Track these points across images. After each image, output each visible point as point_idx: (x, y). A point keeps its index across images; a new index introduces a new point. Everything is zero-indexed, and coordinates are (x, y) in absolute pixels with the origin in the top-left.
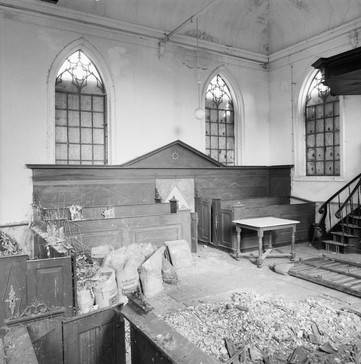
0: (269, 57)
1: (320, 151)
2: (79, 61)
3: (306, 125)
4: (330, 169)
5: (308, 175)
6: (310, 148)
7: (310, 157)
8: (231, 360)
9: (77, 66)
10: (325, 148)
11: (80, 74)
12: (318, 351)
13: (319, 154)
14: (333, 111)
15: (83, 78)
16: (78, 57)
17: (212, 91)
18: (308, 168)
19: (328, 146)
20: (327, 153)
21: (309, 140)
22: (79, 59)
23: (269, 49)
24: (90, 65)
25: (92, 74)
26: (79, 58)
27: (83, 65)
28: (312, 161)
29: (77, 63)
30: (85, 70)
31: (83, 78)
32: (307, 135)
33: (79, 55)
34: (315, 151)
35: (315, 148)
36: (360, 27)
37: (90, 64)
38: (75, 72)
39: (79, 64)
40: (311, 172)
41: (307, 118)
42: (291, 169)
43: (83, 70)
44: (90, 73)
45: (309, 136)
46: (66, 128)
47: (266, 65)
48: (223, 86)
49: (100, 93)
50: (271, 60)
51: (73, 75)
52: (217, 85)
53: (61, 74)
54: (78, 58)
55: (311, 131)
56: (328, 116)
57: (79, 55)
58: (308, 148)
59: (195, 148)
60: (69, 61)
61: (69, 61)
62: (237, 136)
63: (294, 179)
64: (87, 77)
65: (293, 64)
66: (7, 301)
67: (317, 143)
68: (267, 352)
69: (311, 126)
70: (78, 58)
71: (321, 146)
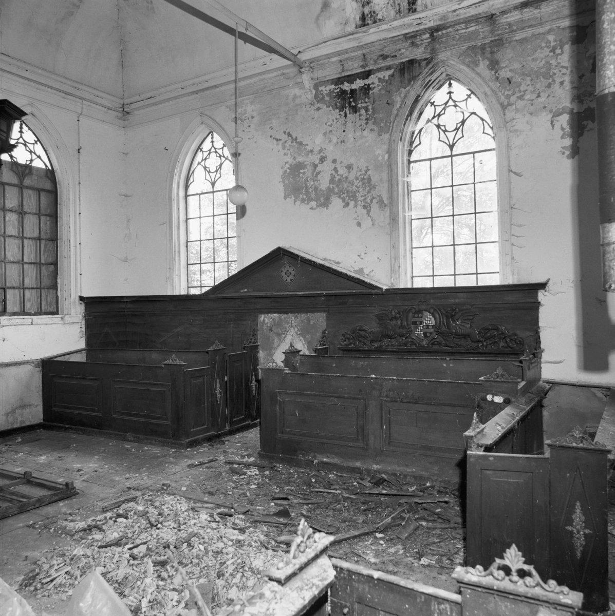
2: (213, 146)
8: (76, 411)
15: (443, 126)
16: (19, 130)
17: (203, 163)
22: (20, 134)
24: (36, 144)
25: (39, 157)
27: (27, 144)
30: (457, 126)
31: (443, 126)
36: (464, 615)
37: (36, 142)
41: (331, 538)
43: (457, 124)
44: (37, 155)
48: (435, 106)
49: (48, 185)
52: (21, 141)
54: (19, 132)
59: (103, 296)
60: (469, 96)
61: (469, 96)
64: (31, 161)
66: (569, 528)
70: (19, 132)
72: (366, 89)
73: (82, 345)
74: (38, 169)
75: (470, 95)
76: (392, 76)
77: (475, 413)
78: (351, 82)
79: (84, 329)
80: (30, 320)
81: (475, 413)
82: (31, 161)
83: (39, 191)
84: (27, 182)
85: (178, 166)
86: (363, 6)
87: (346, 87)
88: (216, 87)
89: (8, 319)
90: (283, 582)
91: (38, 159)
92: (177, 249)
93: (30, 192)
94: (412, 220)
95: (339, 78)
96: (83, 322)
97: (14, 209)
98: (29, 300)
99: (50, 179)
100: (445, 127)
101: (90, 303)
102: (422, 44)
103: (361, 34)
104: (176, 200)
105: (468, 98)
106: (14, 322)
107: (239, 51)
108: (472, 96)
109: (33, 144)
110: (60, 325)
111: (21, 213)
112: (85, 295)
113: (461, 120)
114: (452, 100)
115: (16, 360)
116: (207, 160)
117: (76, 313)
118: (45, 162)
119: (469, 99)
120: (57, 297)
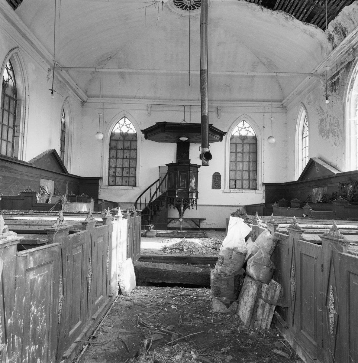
0: (89, 98)
1: (119, 170)
2: (125, 123)
3: (110, 152)
4: (126, 182)
5: (109, 185)
6: (112, 167)
7: (112, 173)
9: (123, 125)
12: (122, 293)
13: (118, 172)
14: (130, 146)
18: (110, 181)
19: (125, 168)
21: (111, 162)
23: (87, 92)
25: (250, 132)
26: (125, 121)
28: (113, 176)
29: (123, 124)
34: (116, 169)
35: (115, 167)
38: (122, 129)
39: (125, 124)
40: (111, 183)
42: (99, 180)
45: (111, 159)
46: (6, 142)
47: (83, 103)
49: (254, 142)
50: (88, 101)
51: (120, 130)
53: (114, 131)
55: (113, 156)
56: (126, 149)
57: (125, 120)
58: (110, 167)
60: (249, 127)
62: (67, 152)
63: (102, 187)
65: (105, 109)
67: (117, 164)
68: (269, 245)
69: (114, 153)
71: (120, 166)
72: (338, 79)
73: (264, 202)
74: (250, 137)
76: (344, 71)
77: (257, 212)
78: (334, 78)
79: (265, 196)
81: (257, 212)
82: (247, 134)
83: (250, 144)
84: (245, 141)
85: (297, 126)
86: (332, 43)
87: (333, 81)
88: (213, 106)
92: (297, 162)
93: (247, 145)
94: (357, 139)
95: (332, 77)
96: (264, 193)
97: (240, 152)
98: (245, 184)
101: (267, 185)
102: (351, 54)
103: (330, 58)
104: (297, 141)
106: (235, 191)
111: (243, 153)
112: (265, 182)
113: (127, 130)
116: (244, 129)
117: (261, 189)
120: (256, 183)
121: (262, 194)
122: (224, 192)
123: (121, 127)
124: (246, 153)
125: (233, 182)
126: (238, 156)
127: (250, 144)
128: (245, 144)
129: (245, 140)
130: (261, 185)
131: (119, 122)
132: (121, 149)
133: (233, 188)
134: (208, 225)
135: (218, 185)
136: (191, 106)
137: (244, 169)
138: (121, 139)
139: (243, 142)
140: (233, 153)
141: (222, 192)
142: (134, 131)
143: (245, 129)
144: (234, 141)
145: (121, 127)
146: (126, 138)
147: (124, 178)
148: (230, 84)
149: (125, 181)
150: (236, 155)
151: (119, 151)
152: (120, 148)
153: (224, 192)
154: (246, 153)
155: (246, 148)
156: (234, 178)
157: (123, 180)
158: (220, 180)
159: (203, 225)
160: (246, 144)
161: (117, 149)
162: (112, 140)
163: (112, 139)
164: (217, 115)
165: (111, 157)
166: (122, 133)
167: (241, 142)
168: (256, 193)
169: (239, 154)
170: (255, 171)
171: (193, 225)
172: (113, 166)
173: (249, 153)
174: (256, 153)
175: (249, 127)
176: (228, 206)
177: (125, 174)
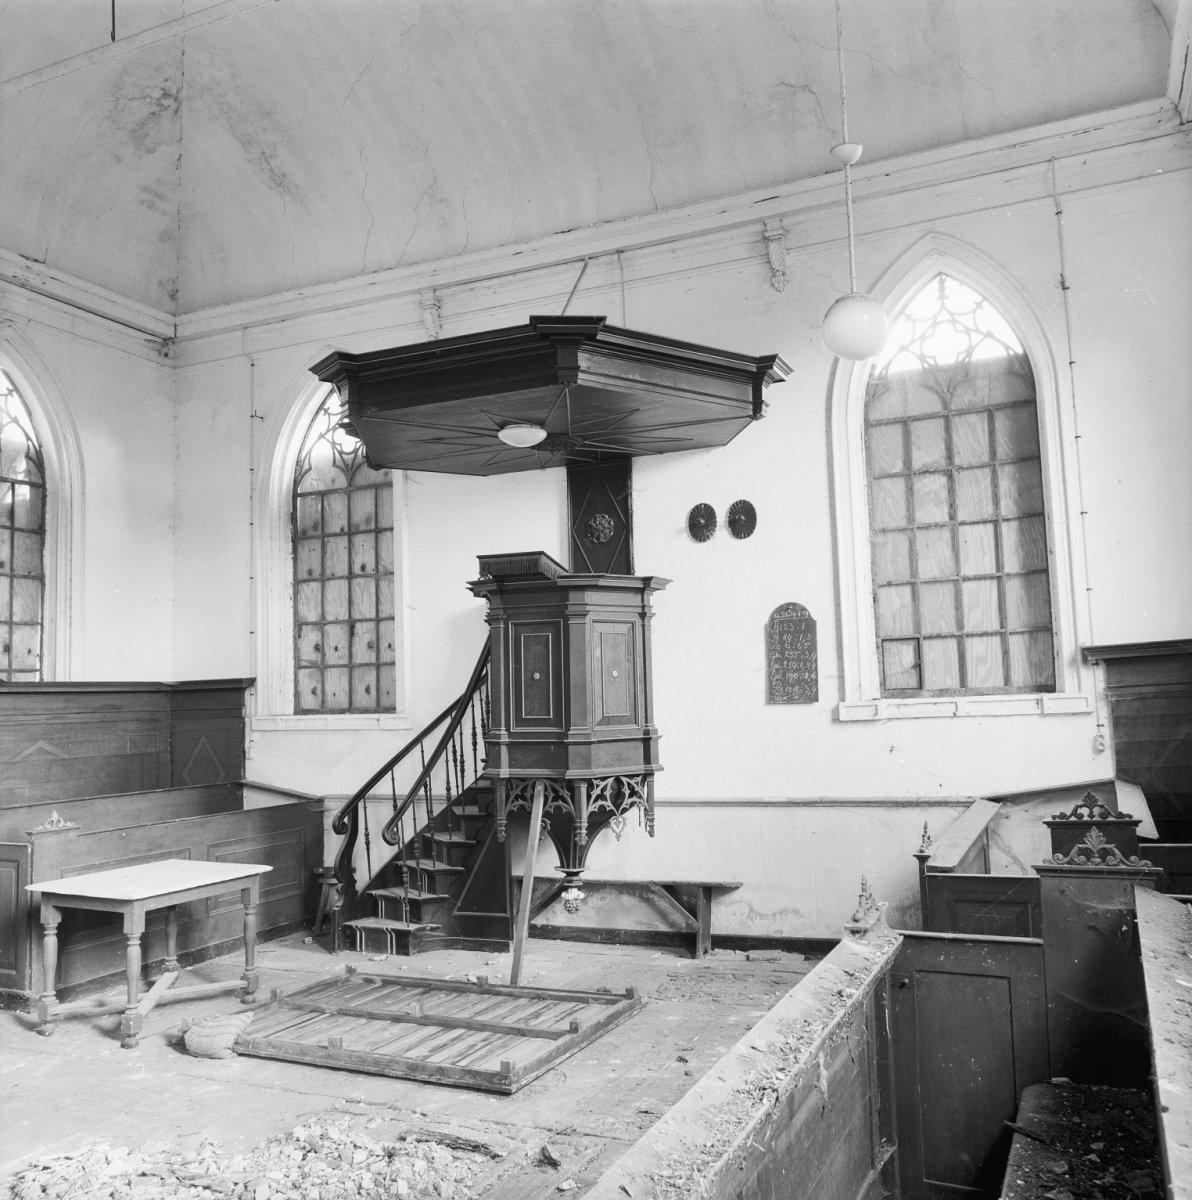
1: (336, 635)
2: (943, 306)
4: (368, 690)
5: (299, 710)
6: (307, 624)
7: (308, 654)
10: (352, 625)
11: (946, 351)
13: (333, 645)
14: (376, 514)
15: (930, 357)
20: (356, 639)
26: (942, 297)
28: (312, 665)
29: (935, 317)
32: (297, 583)
33: (942, 288)
35: (321, 624)
45: (304, 586)
47: (165, 345)
48: (329, 415)
57: (942, 288)
58: (299, 625)
60: (909, 317)
63: (256, 725)
65: (1062, 199)
74: (987, 365)
75: (981, 302)
80: (952, 708)
89: (898, 706)
90: (16, 864)
91: (14, 425)
93: (973, 418)
98: (982, 660)
99: (34, 462)
100: (935, 360)
101: (1116, 659)
105: (976, 309)
106: (906, 711)
107: (124, 318)
108: (985, 304)
109: (5, 395)
110: (1037, 717)
113: (966, 347)
114: (946, 310)
115: (831, 809)
118: (24, 427)
119: (979, 310)
121: (1091, 721)
122: (836, 720)
123: (923, 338)
124: (971, 468)
125: (907, 653)
126: (928, 493)
127: (990, 412)
128: (962, 413)
129: (960, 391)
130: (1073, 661)
131: (326, 407)
132: (342, 533)
133: (901, 693)
134: (762, 916)
135: (799, 682)
136: (620, 251)
137: (967, 570)
138: (337, 485)
139: (945, 404)
140: (891, 476)
141: (828, 717)
142: (1008, 348)
143: (954, 322)
144: (890, 408)
145: (923, 338)
146: (963, 398)
147: (357, 673)
148: (1149, 11)
149: (312, 687)
150: (910, 490)
151: (332, 543)
152: (338, 530)
153: (836, 720)
154: (971, 468)
155: (971, 440)
156: (908, 630)
157: (356, 682)
158: (813, 648)
159: (725, 918)
160: (969, 412)
161: (324, 537)
162: (880, 423)
163: (874, 416)
164: (764, 270)
165: (303, 575)
166: (938, 369)
167: (938, 407)
168: (1043, 715)
169: (928, 480)
170: (1038, 573)
171: (680, 919)
172: (310, 620)
173: (992, 465)
174: (1029, 458)
175: (909, 317)
176: (868, 804)
177: (363, 655)
